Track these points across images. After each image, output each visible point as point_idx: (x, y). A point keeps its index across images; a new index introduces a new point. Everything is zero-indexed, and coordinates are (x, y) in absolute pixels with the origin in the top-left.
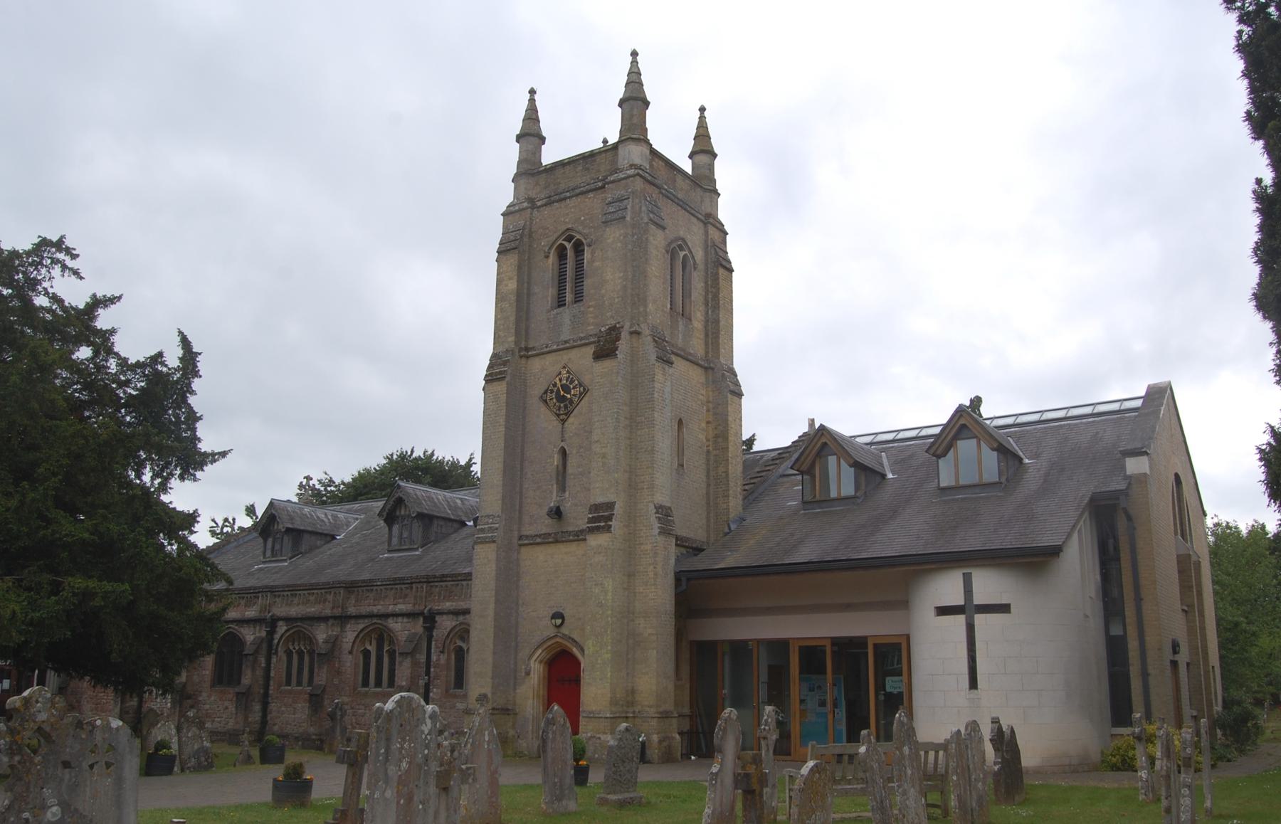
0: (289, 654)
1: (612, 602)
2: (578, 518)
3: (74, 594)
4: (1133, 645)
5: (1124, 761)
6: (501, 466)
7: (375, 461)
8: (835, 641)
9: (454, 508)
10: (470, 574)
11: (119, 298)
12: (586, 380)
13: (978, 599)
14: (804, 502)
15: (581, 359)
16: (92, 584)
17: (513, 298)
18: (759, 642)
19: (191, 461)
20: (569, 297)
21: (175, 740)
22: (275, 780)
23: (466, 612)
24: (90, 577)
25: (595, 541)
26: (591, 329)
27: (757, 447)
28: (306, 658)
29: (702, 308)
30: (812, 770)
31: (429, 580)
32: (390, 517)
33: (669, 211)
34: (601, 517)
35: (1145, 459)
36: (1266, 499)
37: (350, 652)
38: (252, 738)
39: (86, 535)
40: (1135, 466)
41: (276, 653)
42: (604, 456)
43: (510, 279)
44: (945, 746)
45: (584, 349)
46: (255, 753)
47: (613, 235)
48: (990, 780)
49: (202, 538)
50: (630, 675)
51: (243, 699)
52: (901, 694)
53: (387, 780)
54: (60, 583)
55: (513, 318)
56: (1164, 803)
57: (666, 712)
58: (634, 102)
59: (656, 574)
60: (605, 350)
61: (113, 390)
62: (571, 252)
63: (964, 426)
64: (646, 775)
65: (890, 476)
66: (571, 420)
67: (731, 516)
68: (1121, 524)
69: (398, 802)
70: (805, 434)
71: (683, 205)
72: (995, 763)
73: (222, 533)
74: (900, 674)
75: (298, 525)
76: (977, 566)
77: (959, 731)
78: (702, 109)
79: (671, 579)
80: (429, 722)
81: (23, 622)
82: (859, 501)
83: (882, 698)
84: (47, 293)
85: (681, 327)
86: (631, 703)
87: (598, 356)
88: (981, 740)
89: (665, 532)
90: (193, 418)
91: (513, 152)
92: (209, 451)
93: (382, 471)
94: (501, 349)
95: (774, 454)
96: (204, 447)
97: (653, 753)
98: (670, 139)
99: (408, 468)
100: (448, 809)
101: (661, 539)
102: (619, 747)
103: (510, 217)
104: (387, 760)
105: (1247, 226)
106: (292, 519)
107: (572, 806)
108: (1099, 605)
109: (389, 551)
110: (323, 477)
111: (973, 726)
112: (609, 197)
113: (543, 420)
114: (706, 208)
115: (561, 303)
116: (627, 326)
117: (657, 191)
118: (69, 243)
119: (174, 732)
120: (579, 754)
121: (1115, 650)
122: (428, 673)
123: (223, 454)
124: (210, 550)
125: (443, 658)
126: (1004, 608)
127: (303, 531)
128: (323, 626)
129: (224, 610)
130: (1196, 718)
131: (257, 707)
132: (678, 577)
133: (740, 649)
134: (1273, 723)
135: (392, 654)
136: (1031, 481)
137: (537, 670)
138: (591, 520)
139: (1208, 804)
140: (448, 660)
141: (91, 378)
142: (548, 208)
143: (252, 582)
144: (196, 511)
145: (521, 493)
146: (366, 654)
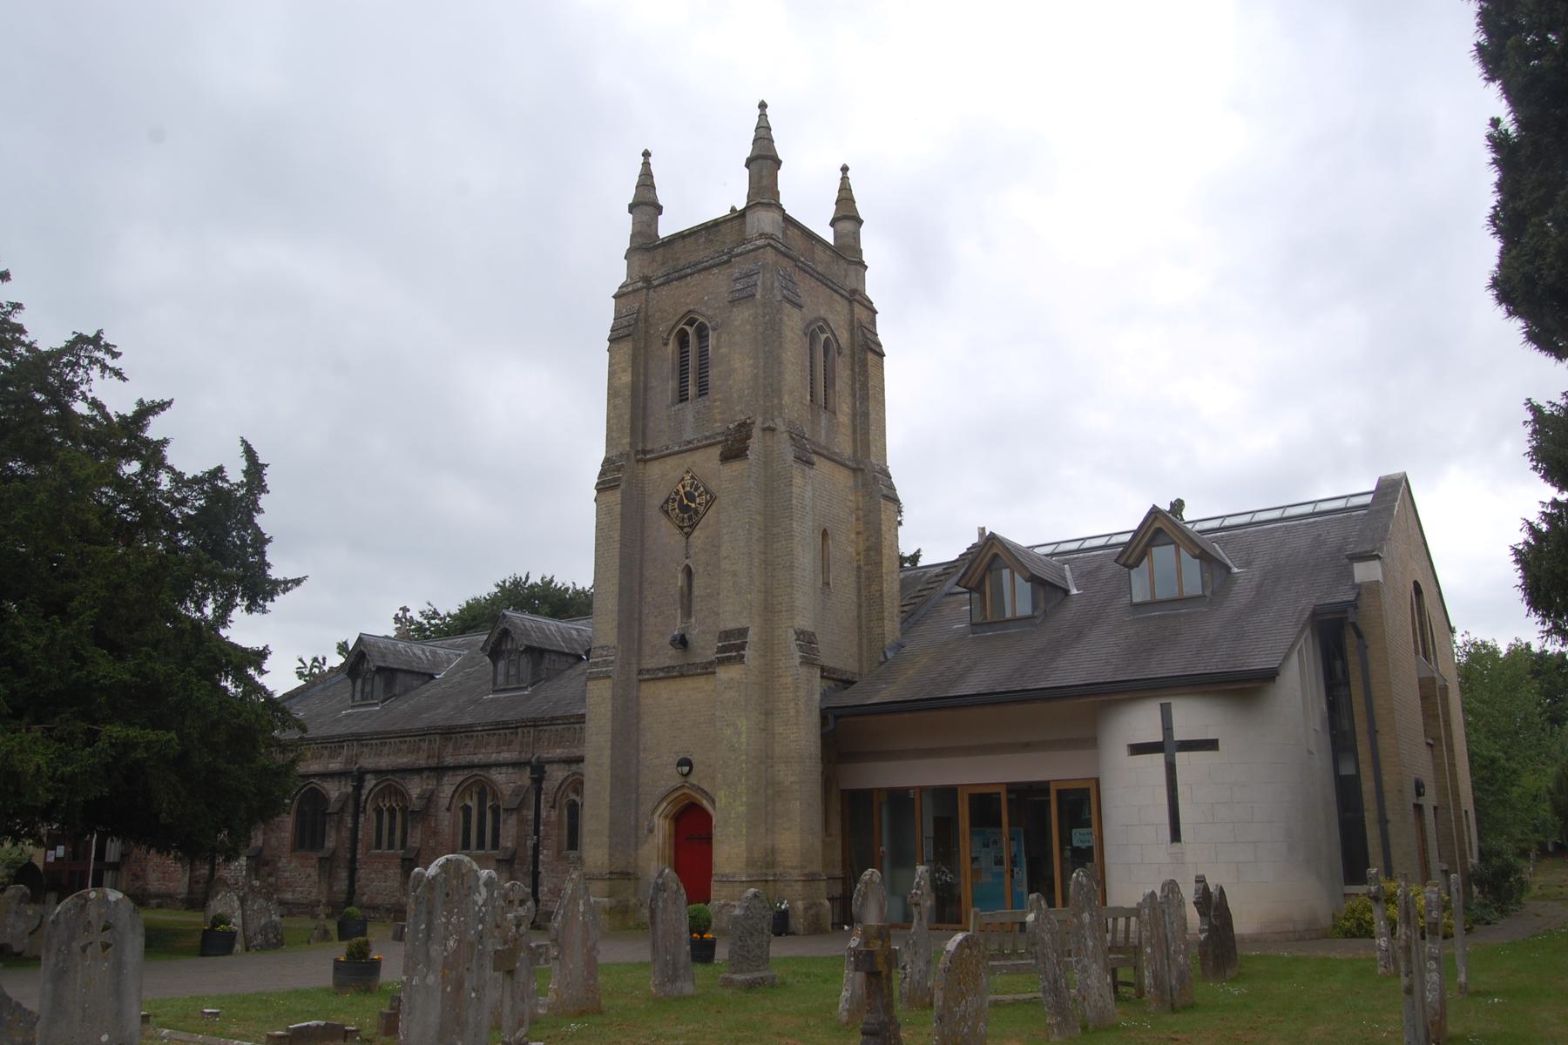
0: (379, 812)
1: (746, 742)
2: (705, 647)
3: (112, 745)
4: (1368, 786)
5: (1359, 926)
6: (616, 589)
7: (485, 589)
8: (1012, 788)
9: (569, 640)
10: (583, 716)
11: (169, 403)
12: (713, 485)
13: (1179, 735)
14: (973, 625)
15: (707, 462)
16: (133, 732)
17: (627, 393)
18: (922, 789)
19: (259, 589)
20: (692, 390)
21: (238, 913)
22: (336, 961)
23: (580, 760)
24: (133, 725)
25: (725, 674)
26: (718, 427)
27: (922, 562)
28: (399, 815)
29: (849, 400)
30: (960, 944)
31: (536, 723)
32: (495, 652)
33: (806, 288)
34: (732, 646)
35: (1376, 564)
36: (1524, 607)
37: (448, 809)
38: (329, 911)
39: (127, 677)
40: (1364, 572)
41: (364, 811)
42: (735, 574)
43: (624, 371)
44: (1136, 912)
45: (710, 450)
46: (332, 926)
47: (742, 317)
48: (1195, 951)
49: (279, 679)
50: (769, 832)
51: (327, 865)
52: (1090, 849)
53: (428, 962)
54: (98, 732)
55: (627, 417)
56: (1404, 981)
57: (813, 874)
58: (763, 161)
59: (797, 711)
60: (734, 450)
61: (167, 510)
62: (692, 337)
63: (1159, 530)
64: (780, 949)
65: (1074, 591)
66: (696, 533)
67: (887, 642)
68: (1350, 641)
69: (444, 990)
70: (974, 546)
71: (823, 280)
72: (1201, 931)
73: (311, 674)
74: (1088, 824)
75: (391, 662)
76: (1176, 695)
77: (1153, 893)
78: (845, 169)
79: (815, 718)
80: (483, 890)
81: (50, 779)
82: (1038, 621)
83: (1068, 854)
84: (85, 398)
85: (823, 423)
86: (772, 865)
87: (726, 458)
88: (1181, 903)
89: (808, 662)
90: (261, 541)
91: (624, 225)
92: (281, 578)
93: (494, 601)
94: (615, 452)
95: (939, 570)
96: (275, 573)
97: (797, 923)
98: (807, 201)
99: (518, 595)
100: (513, 998)
101: (803, 671)
102: (746, 917)
103: (623, 300)
104: (428, 937)
105: (1480, 185)
106: (383, 656)
107: (688, 988)
108: (1326, 740)
109: (495, 692)
110: (426, 608)
111: (1171, 887)
112: (736, 273)
113: (664, 534)
114: (850, 283)
115: (683, 397)
116: (759, 421)
117: (792, 263)
118: (107, 338)
119: (237, 904)
120: (699, 925)
121: (1347, 793)
122: (537, 832)
123: (298, 582)
124: (290, 696)
125: (554, 814)
126: (1211, 745)
127: (397, 670)
128: (416, 779)
129: (293, 762)
130: (1446, 873)
131: (344, 874)
132: (825, 714)
133: (900, 799)
134: (1541, 877)
135: (496, 811)
136: (1241, 594)
137: (662, 827)
138: (720, 650)
139: (1462, 978)
140: (560, 816)
141: (140, 494)
142: (666, 288)
143: (340, 730)
144: (266, 648)
145: (640, 619)
146: (467, 810)
